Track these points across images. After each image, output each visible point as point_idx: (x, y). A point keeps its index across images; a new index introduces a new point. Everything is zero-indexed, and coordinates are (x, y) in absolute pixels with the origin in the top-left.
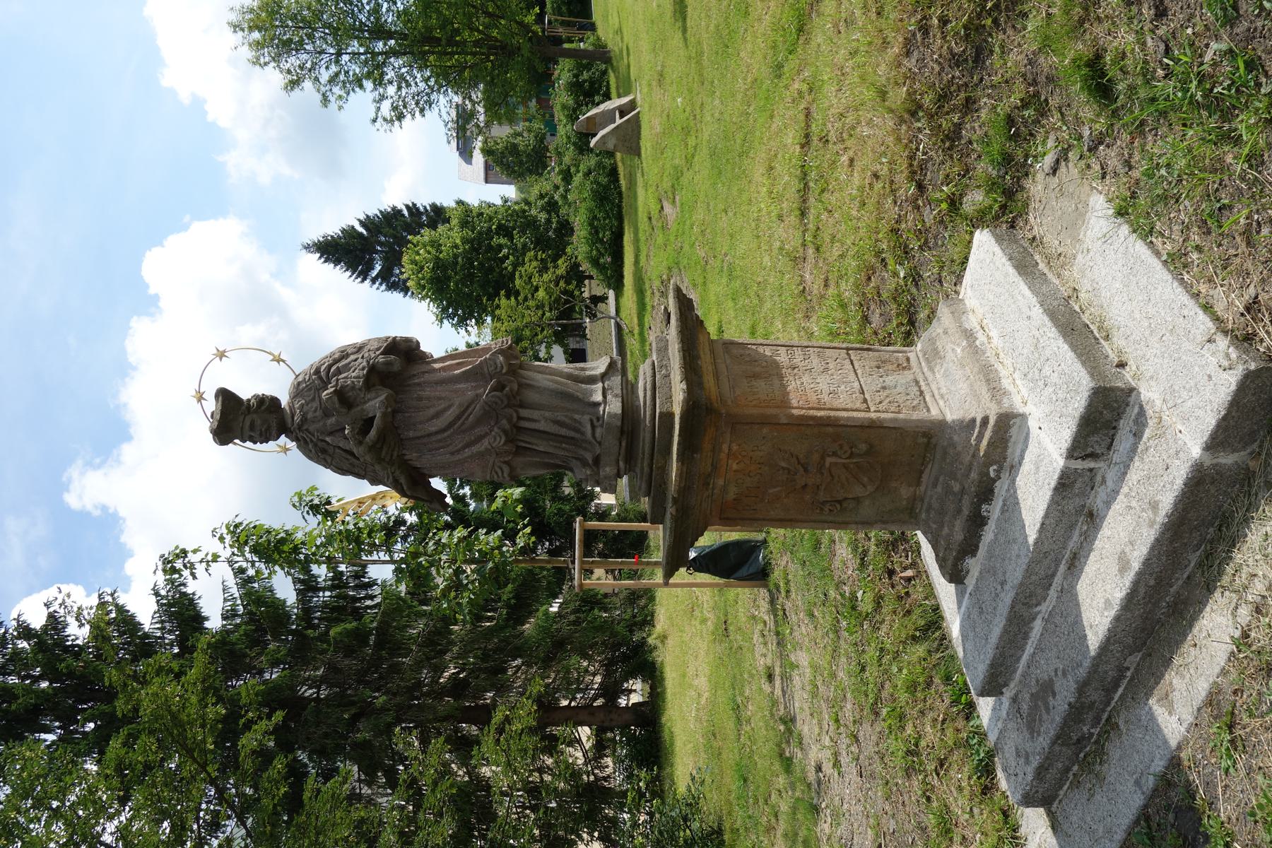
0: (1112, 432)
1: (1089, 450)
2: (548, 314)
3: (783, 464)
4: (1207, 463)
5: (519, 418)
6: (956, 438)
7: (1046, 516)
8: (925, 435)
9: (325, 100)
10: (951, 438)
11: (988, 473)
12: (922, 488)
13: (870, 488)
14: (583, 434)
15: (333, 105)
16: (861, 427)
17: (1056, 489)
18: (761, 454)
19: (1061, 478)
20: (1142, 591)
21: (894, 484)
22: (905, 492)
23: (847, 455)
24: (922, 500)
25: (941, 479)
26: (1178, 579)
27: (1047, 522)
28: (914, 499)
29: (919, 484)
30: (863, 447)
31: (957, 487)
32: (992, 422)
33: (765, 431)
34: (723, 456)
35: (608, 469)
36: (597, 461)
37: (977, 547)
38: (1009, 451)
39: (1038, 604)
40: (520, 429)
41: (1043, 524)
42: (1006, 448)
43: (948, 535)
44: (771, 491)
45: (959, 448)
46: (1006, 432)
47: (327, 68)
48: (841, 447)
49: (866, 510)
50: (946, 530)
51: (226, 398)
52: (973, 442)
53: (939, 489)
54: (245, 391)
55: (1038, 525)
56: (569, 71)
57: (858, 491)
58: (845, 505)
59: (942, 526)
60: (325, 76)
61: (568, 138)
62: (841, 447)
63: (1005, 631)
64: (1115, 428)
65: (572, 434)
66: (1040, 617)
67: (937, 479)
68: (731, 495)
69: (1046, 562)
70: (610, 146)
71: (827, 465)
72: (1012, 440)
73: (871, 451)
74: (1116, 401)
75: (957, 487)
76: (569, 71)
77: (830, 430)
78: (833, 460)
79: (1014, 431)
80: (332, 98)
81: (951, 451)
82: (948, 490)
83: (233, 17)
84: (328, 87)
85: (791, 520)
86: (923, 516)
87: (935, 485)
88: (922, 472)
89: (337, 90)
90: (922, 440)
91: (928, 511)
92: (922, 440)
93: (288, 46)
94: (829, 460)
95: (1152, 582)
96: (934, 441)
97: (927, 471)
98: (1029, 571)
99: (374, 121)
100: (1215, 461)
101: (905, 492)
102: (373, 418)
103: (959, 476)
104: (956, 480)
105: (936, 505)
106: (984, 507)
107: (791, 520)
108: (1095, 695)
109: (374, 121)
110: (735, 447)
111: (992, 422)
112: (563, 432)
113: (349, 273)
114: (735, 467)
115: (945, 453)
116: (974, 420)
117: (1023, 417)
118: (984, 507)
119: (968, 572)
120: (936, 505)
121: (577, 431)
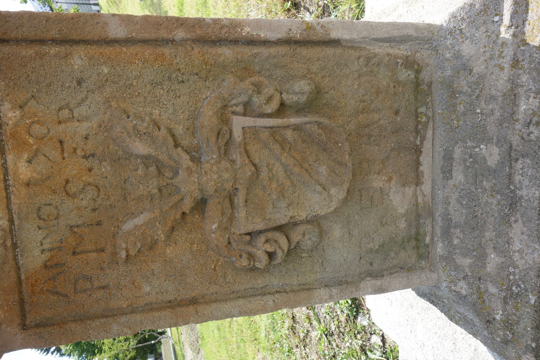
2: (132, 343)
3: (141, 148)
10: (458, 56)
12: (426, 187)
13: (338, 194)
16: (288, 42)
18: (83, 128)
22: (399, 200)
23: (274, 106)
24: (431, 214)
25: (458, 153)
28: (419, 215)
29: (418, 182)
31: (492, 155)
43: (502, 267)
44: (128, 226)
45: (479, 68)
49: (341, 250)
50: (493, 260)
52: (505, 34)
53: (458, 176)
58: (296, 237)
59: (482, 257)
67: (448, 158)
68: (34, 258)
75: (492, 155)
77: (227, 53)
78: (249, 121)
81: (463, 84)
82: (477, 169)
85: (194, 302)
86: (440, 249)
87: (447, 173)
88: (418, 151)
90: (405, 75)
91: (447, 234)
92: (405, 75)
97: (427, 145)
101: (399, 200)
103: (492, 129)
104: (488, 141)
105: (458, 215)
107: (194, 302)
113: (39, 351)
120: (458, 215)
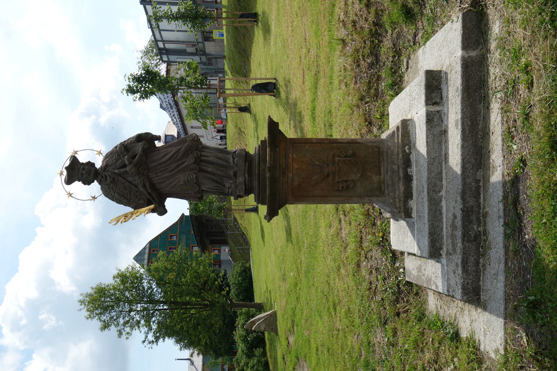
0: (440, 91)
1: (434, 101)
4: (466, 56)
5: (201, 156)
6: (389, 144)
7: (427, 137)
8: (377, 147)
9: (120, 334)
10: (388, 146)
11: (405, 151)
12: (382, 176)
13: (359, 175)
14: (229, 163)
15: (124, 336)
16: (348, 143)
17: (427, 122)
19: (427, 116)
20: (467, 128)
21: (369, 174)
22: (375, 179)
24: (384, 183)
26: (480, 121)
27: (428, 140)
30: (350, 152)
31: (395, 167)
32: (400, 126)
33: (307, 146)
34: (290, 160)
35: (240, 179)
36: (235, 174)
37: (412, 193)
38: (411, 138)
39: (440, 191)
40: (201, 161)
41: (427, 142)
42: (409, 136)
44: (314, 178)
46: (407, 129)
47: (123, 318)
48: (341, 152)
51: (74, 160)
53: (389, 173)
54: (83, 159)
55: (425, 143)
56: (243, 319)
57: (353, 177)
60: (121, 321)
61: (243, 351)
62: (341, 152)
63: (430, 210)
64: (440, 89)
65: (224, 163)
66: (443, 199)
67: (387, 169)
68: (296, 183)
69: (436, 164)
70: (262, 328)
71: (336, 161)
72: (411, 132)
73: (353, 155)
74: (436, 76)
75: (395, 167)
76: (243, 319)
77: (335, 145)
79: (410, 128)
80: (124, 333)
81: (389, 152)
83: (81, 298)
84: (122, 328)
88: (380, 168)
89: (128, 329)
92: (376, 150)
93: (105, 309)
94: (337, 159)
95: (469, 123)
96: (381, 150)
97: (382, 166)
98: (430, 171)
99: (144, 342)
100: (468, 55)
102: (137, 155)
106: (409, 170)
108: (471, 202)
109: (144, 342)
110: (295, 156)
111: (400, 126)
112: (220, 162)
114: (296, 166)
115: (387, 154)
116: (394, 132)
117: (411, 120)
118: (409, 170)
119: (412, 209)
120: (390, 183)
121: (227, 162)
